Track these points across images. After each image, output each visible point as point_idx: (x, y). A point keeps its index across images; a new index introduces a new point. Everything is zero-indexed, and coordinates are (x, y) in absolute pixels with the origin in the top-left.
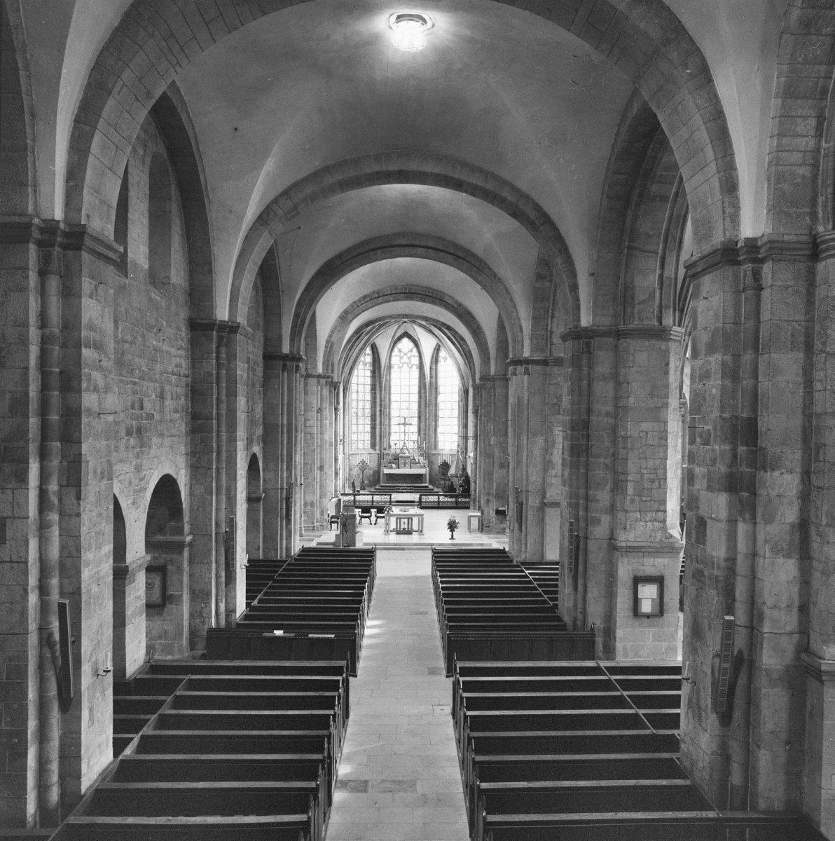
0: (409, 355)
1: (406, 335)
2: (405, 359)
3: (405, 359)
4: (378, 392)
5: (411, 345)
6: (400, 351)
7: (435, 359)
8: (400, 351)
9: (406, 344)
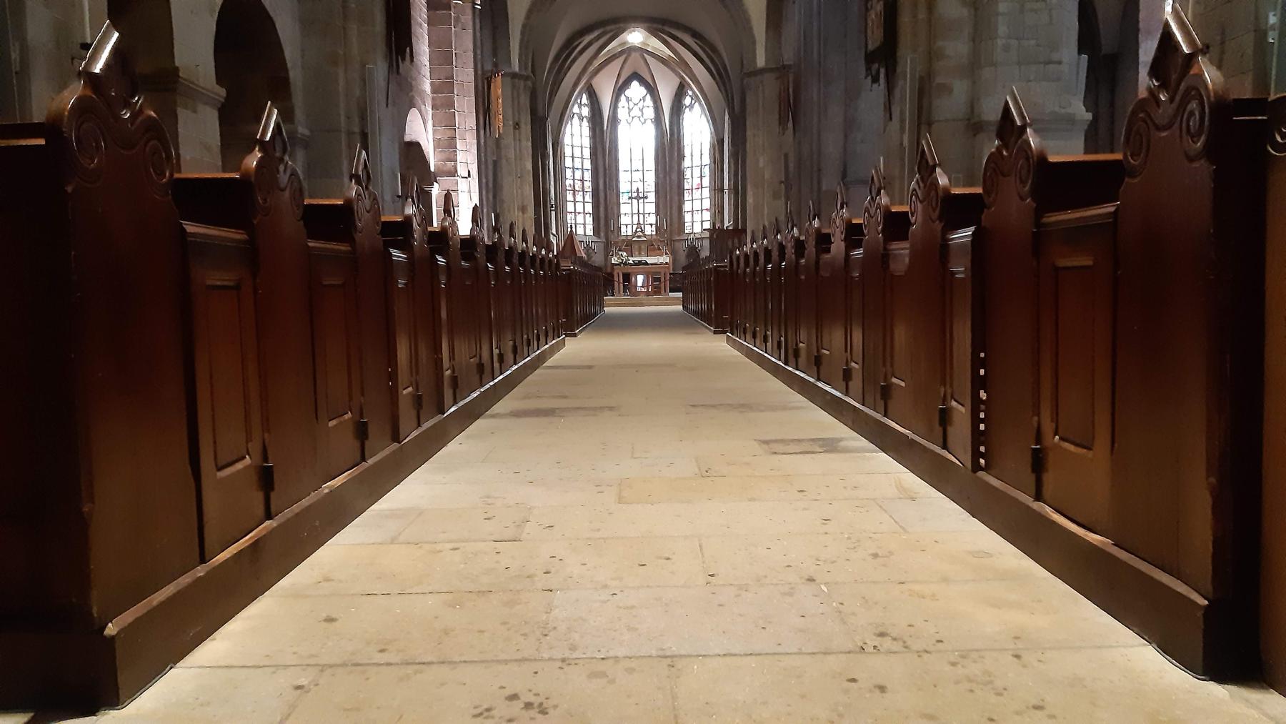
0: (640, 105)
1: (636, 76)
2: (636, 112)
3: (636, 112)
4: (600, 157)
5: (643, 91)
6: (628, 99)
7: (677, 109)
8: (628, 99)
9: (636, 90)
